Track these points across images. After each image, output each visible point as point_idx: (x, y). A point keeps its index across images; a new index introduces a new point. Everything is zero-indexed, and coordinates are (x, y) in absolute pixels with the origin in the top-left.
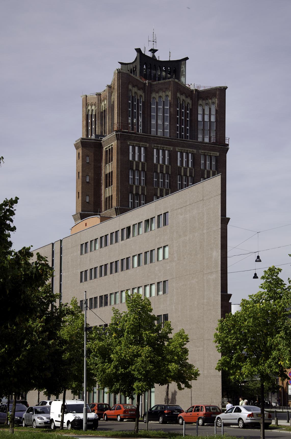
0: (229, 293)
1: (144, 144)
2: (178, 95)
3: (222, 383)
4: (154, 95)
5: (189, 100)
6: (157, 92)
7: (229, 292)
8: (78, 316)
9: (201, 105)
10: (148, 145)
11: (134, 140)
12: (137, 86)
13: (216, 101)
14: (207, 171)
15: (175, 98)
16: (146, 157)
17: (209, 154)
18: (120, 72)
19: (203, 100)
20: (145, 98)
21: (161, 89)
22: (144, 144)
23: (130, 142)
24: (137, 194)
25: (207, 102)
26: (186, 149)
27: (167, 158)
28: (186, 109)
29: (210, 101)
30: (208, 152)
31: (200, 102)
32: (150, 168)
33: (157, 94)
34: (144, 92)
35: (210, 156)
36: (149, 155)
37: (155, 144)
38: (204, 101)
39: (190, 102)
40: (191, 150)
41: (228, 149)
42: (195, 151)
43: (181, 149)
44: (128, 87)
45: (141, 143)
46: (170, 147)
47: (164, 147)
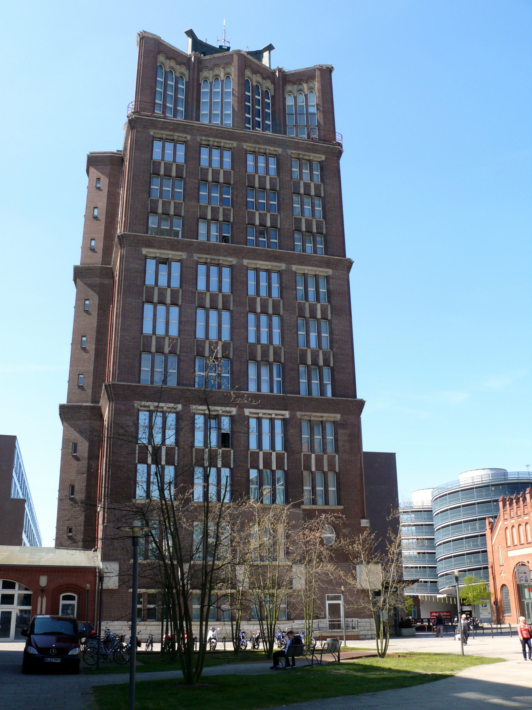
0: (359, 396)
1: (181, 135)
2: (248, 73)
4: (205, 74)
7: (372, 442)
8: (318, 558)
9: (290, 92)
10: (189, 137)
11: (162, 129)
12: (174, 59)
14: (305, 183)
17: (307, 158)
18: (143, 38)
19: (294, 84)
20: (189, 76)
21: (217, 65)
22: (181, 135)
23: (156, 131)
24: (166, 214)
25: (300, 87)
26: (263, 147)
30: (303, 153)
31: (289, 88)
32: (289, 362)
33: (211, 72)
35: (309, 160)
37: (201, 135)
38: (295, 86)
39: (271, 87)
40: (272, 148)
43: (254, 145)
45: (177, 134)
46: (232, 142)
47: (220, 143)
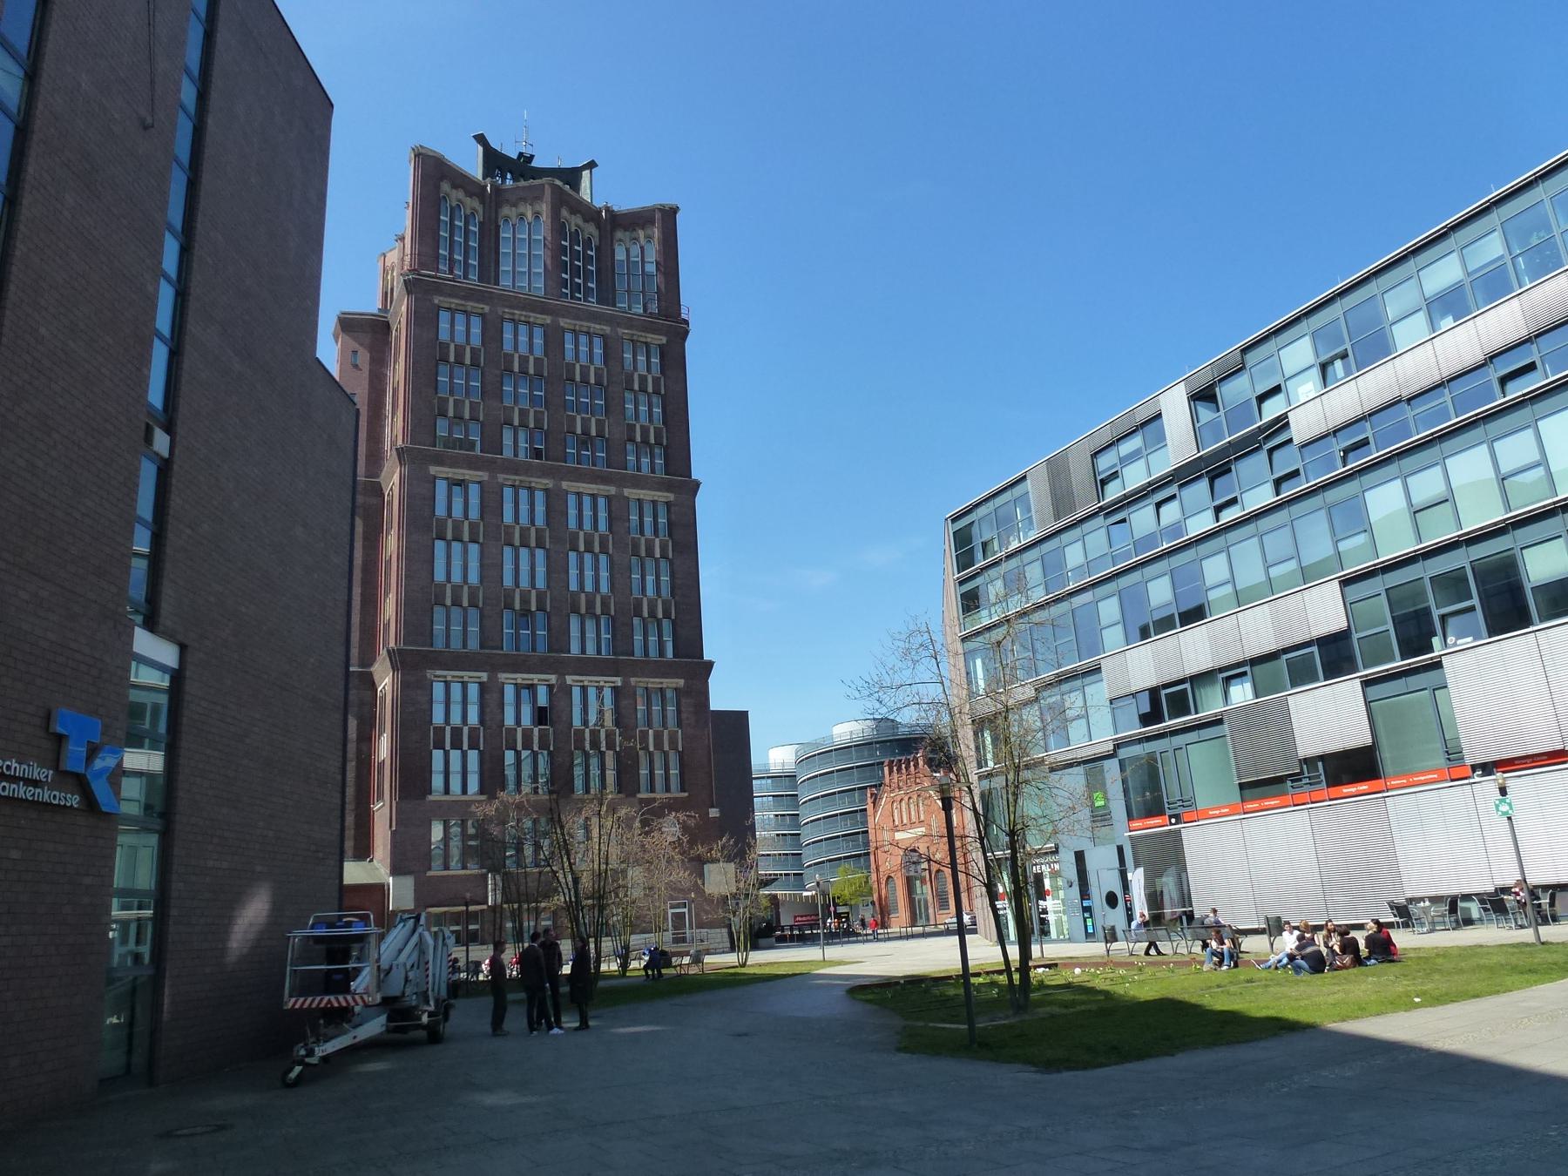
2: (564, 213)
3: (1180, 1002)
4: (506, 210)
5: (591, 229)
6: (515, 205)
10: (487, 309)
11: (450, 296)
13: (656, 232)
15: (559, 229)
16: (617, 710)
19: (626, 230)
21: (524, 200)
25: (634, 235)
27: (604, 574)
28: (587, 244)
29: (641, 233)
34: (482, 202)
36: (492, 333)
39: (596, 233)
41: (687, 332)
42: (607, 329)
44: (438, 188)
